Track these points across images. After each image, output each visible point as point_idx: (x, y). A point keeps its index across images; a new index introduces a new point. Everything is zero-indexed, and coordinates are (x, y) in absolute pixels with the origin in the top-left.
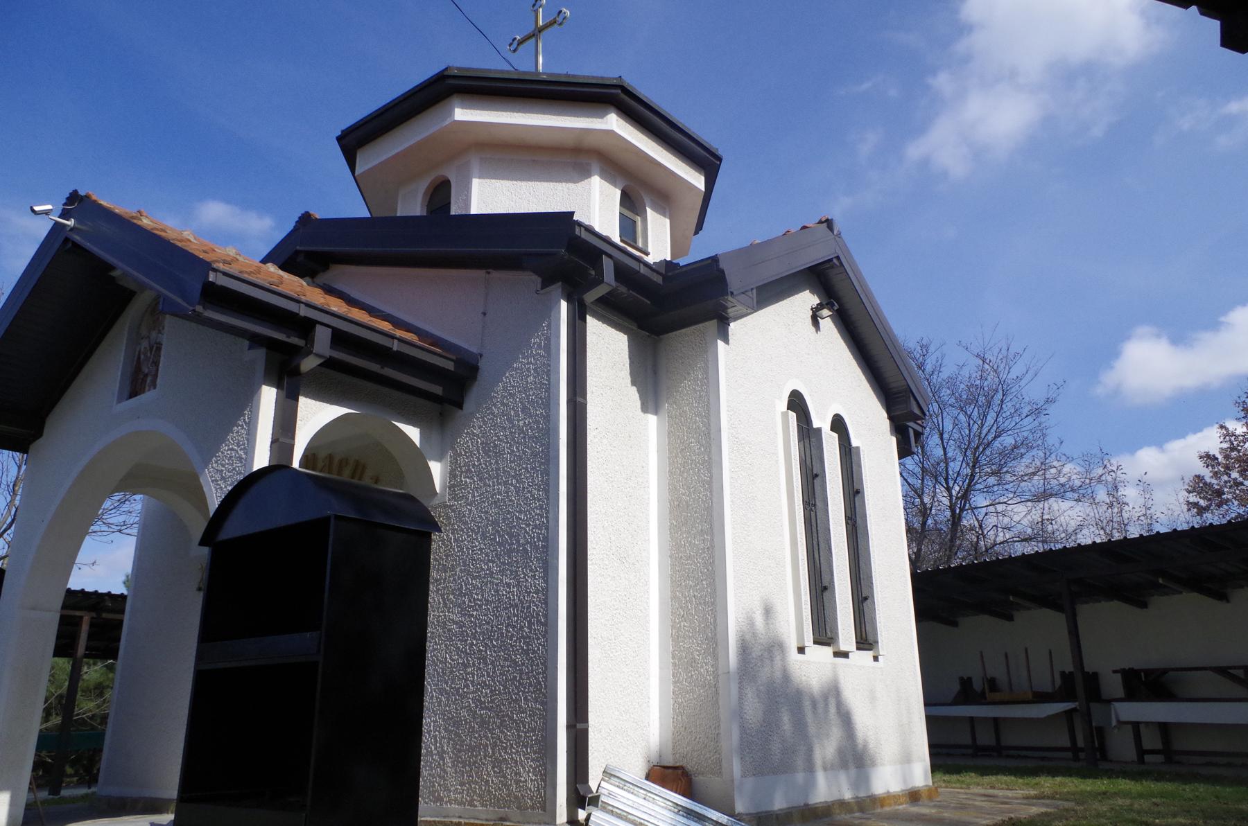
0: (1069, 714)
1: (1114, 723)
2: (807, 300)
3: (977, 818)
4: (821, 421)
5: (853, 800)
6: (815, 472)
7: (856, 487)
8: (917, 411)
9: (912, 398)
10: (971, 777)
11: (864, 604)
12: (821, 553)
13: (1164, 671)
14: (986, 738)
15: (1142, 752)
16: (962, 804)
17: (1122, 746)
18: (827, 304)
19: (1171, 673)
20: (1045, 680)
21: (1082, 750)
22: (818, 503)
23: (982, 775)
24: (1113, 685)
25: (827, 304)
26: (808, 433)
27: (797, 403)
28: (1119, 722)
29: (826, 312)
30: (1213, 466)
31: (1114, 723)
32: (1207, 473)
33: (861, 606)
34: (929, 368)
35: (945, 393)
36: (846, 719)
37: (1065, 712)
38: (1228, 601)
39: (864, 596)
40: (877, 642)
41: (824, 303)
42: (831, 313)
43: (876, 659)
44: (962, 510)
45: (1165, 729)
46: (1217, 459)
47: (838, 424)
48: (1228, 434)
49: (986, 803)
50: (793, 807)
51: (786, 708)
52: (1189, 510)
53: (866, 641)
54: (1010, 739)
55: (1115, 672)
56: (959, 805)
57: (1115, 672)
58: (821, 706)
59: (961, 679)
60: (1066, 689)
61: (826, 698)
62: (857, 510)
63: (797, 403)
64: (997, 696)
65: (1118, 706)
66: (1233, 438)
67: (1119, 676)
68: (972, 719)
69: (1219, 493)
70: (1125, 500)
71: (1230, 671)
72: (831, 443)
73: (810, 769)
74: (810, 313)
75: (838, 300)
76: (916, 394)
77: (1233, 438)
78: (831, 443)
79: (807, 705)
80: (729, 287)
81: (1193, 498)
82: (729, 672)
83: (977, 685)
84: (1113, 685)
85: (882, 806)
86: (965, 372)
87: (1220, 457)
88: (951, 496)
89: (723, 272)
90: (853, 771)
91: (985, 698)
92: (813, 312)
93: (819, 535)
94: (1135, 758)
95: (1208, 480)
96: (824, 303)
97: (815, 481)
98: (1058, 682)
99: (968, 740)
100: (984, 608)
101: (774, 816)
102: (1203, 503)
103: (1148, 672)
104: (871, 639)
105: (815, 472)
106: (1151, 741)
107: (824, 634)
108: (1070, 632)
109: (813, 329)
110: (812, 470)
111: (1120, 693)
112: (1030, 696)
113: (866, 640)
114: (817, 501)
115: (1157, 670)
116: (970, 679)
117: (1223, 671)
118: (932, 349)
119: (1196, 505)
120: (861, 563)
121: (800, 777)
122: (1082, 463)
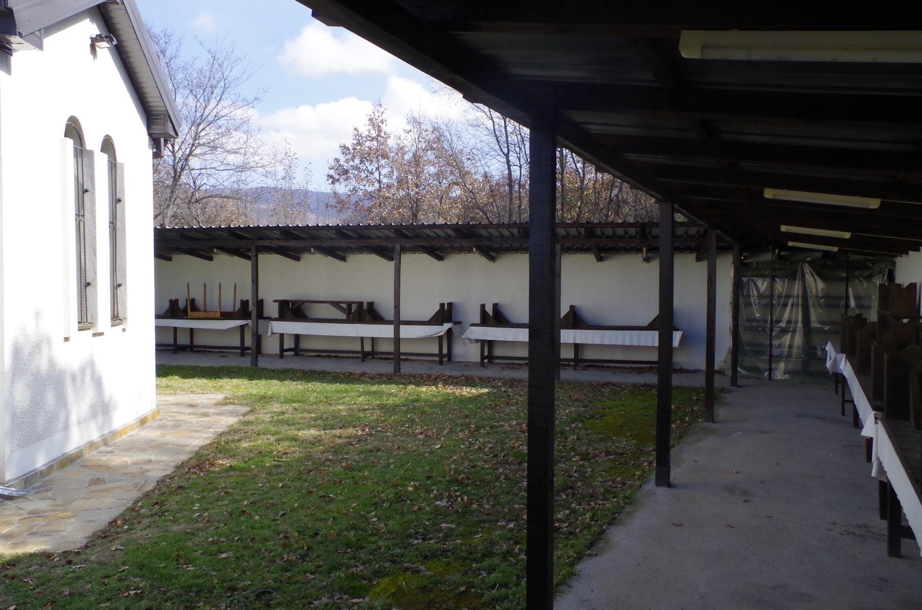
0: (242, 328)
1: (269, 334)
2: (89, 28)
3: (191, 437)
4: (93, 143)
5: (98, 440)
6: (85, 188)
7: (118, 196)
8: (172, 133)
9: (169, 122)
10: (176, 380)
11: (118, 290)
12: (87, 256)
13: (303, 302)
14: (183, 340)
15: (282, 350)
16: (177, 421)
17: (271, 346)
18: (106, 37)
19: (306, 304)
20: (229, 305)
21: (249, 348)
22: (86, 214)
23: (184, 377)
24: (272, 309)
25: (106, 37)
26: (81, 151)
27: (73, 130)
28: (272, 333)
29: (104, 44)
30: (346, 155)
31: (269, 334)
32: (342, 159)
33: (115, 291)
34: (168, 53)
35: (180, 76)
36: (98, 383)
37: (241, 326)
38: (345, 261)
39: (118, 283)
40: (125, 319)
41: (103, 36)
42: (109, 46)
43: (124, 330)
44: (182, 169)
45: (297, 337)
46: (349, 149)
47: (108, 145)
48: (357, 135)
49: (191, 416)
50: (53, 460)
51: (52, 387)
52: (328, 180)
53: (116, 318)
54: (199, 341)
55: (275, 301)
56: (6, 51)
57: (275, 301)
58: (78, 378)
59: (171, 301)
60: (243, 312)
61: (83, 370)
62: (118, 215)
63: (73, 130)
64: (196, 314)
65: (274, 323)
66: (360, 138)
67: (277, 304)
68: (175, 328)
69: (346, 172)
70: (294, 175)
71: (341, 305)
72: (101, 161)
73: (66, 427)
74: (89, 42)
75: (117, 37)
76: (172, 119)
77: (360, 138)
78: (101, 161)
79: (68, 380)
80: (17, 27)
81: (332, 172)
82: (4, 373)
83: (182, 305)
84: (272, 309)
85: (121, 436)
86: (198, 65)
87: (351, 148)
88: (174, 156)
89: (11, 11)
90: (100, 418)
91: (187, 315)
92: (92, 40)
93: (86, 240)
94: (278, 353)
95: (342, 162)
96: (103, 36)
97: (85, 195)
98: (238, 306)
99: (171, 341)
100: (193, 252)
101: (39, 473)
102: (337, 177)
103: (294, 302)
104: (121, 316)
105: (85, 188)
106: (290, 343)
107: (85, 321)
108: (253, 281)
109: (91, 57)
110: (83, 185)
111: (276, 314)
112: (218, 315)
113: (118, 317)
114: (86, 212)
115: (300, 301)
116: (177, 301)
117: (336, 304)
118: (174, 39)
119: (331, 177)
120: (117, 257)
121: (58, 436)
122: (271, 148)
